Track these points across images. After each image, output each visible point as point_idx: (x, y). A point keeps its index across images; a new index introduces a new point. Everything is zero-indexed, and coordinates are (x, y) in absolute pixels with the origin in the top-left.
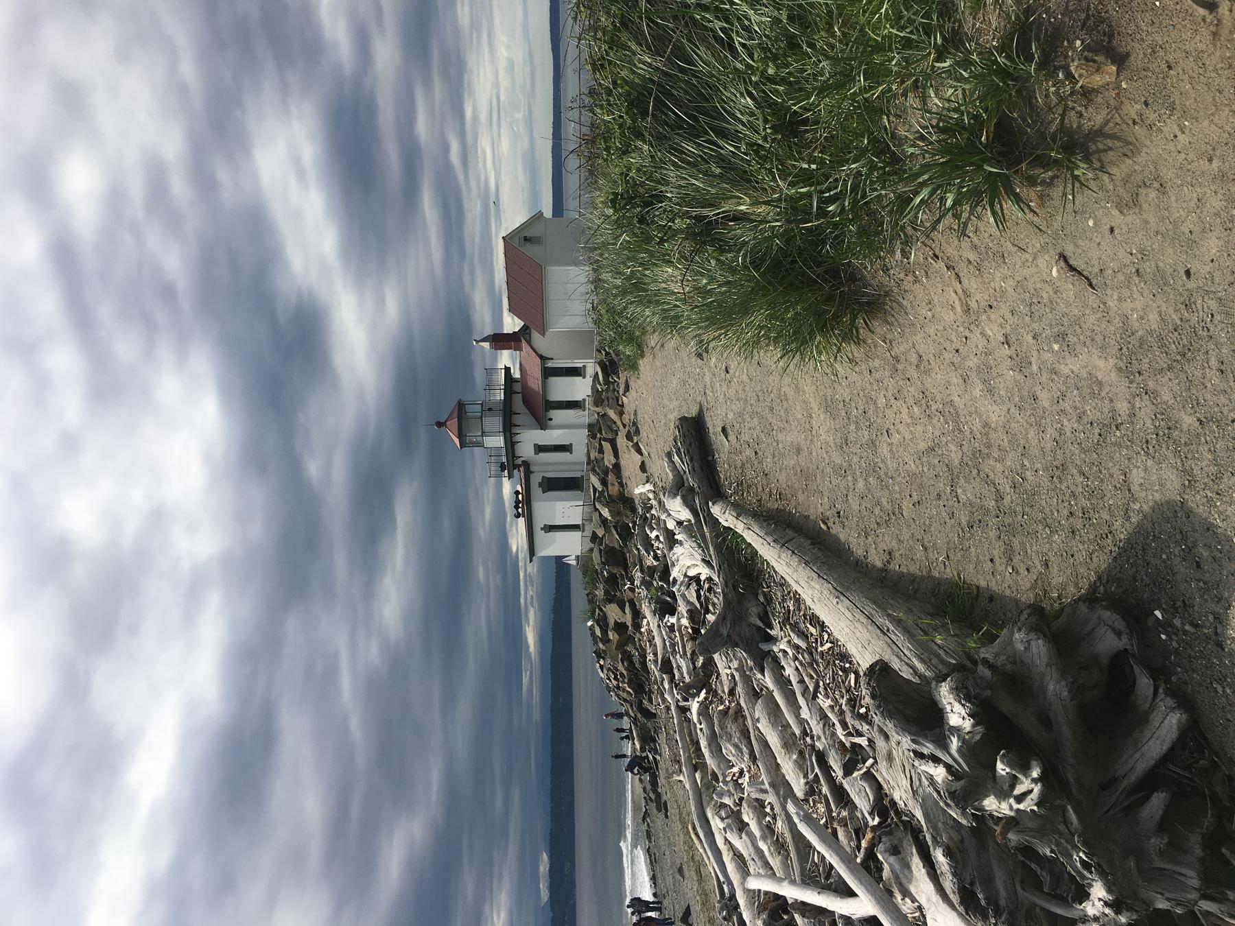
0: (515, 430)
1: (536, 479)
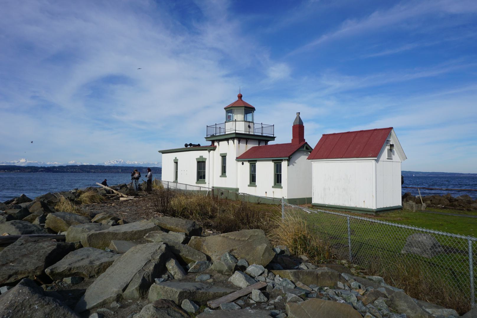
0: (236, 141)
1: (204, 154)
